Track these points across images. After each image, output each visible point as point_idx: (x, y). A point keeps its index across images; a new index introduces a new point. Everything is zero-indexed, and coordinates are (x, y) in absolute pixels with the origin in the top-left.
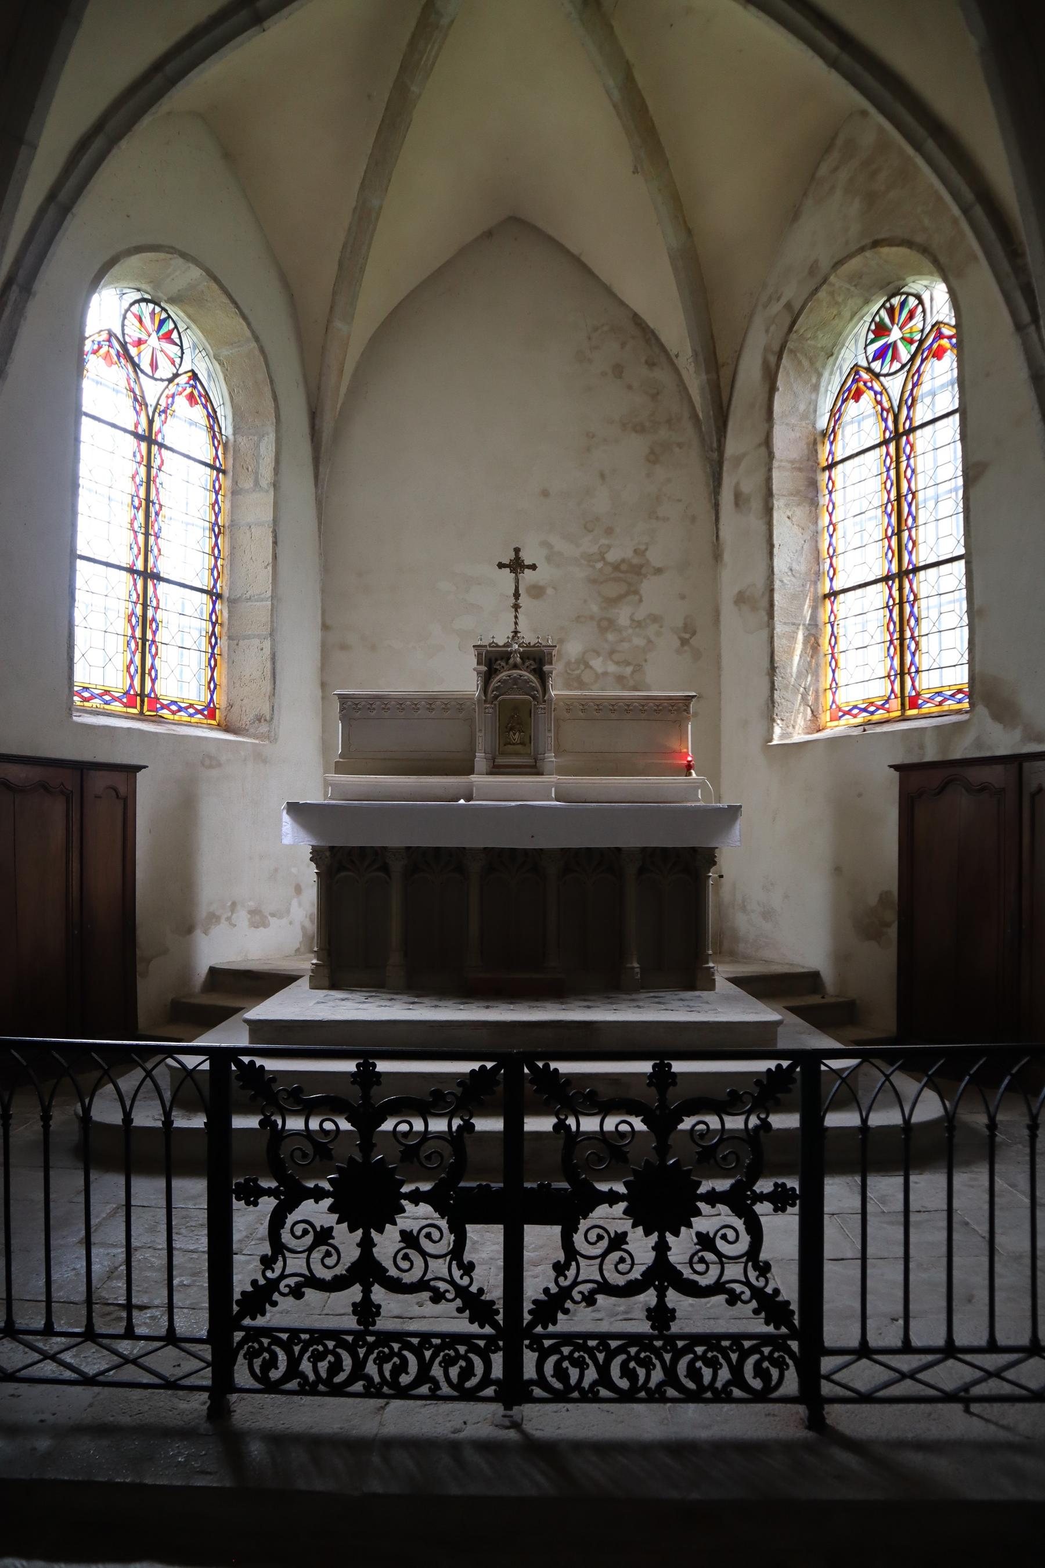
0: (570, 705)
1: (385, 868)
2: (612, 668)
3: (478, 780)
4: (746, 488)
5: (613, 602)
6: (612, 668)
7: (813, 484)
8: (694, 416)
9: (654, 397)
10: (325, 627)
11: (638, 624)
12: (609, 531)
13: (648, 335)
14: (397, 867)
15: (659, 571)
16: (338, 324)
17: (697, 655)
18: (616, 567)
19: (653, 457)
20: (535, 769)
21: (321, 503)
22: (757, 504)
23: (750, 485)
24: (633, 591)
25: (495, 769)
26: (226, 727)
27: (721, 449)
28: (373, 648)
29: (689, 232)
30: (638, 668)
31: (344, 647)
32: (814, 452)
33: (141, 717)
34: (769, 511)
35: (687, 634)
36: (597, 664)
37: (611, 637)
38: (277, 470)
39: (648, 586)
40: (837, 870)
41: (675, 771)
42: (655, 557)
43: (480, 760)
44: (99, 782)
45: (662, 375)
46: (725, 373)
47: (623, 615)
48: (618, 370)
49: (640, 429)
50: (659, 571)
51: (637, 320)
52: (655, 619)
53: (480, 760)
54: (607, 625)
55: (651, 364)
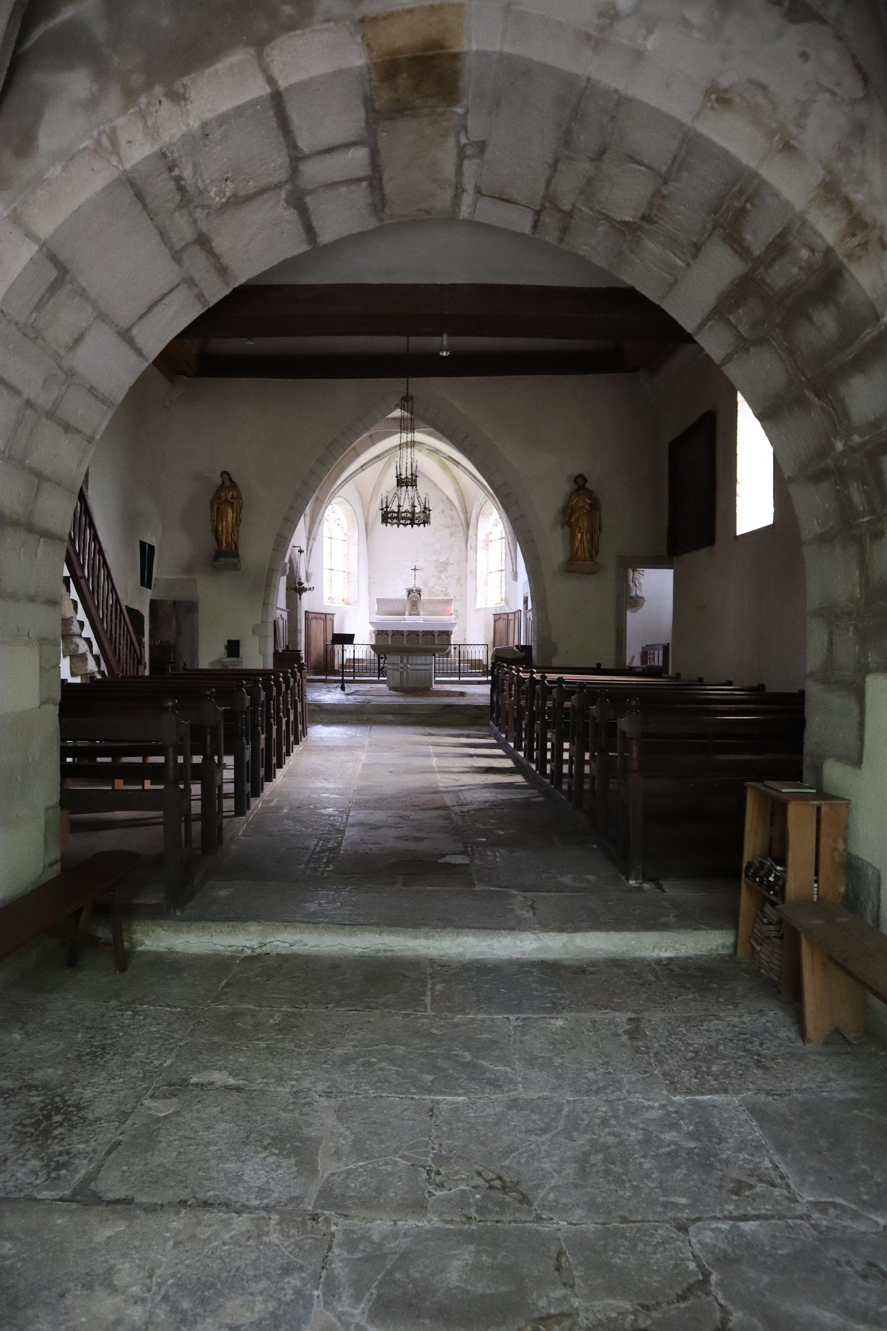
0: (427, 601)
1: (387, 635)
2: (440, 589)
3: (406, 617)
4: (473, 545)
5: (441, 572)
6: (440, 589)
7: (487, 545)
8: (462, 524)
9: (452, 519)
10: (369, 578)
11: (447, 578)
12: (440, 554)
13: (451, 502)
14: (390, 634)
15: (452, 564)
16: (373, 504)
17: (461, 585)
18: (442, 563)
19: (451, 535)
20: (418, 615)
21: (368, 546)
22: (474, 550)
23: (473, 545)
24: (445, 569)
25: (410, 615)
26: (347, 604)
27: (468, 534)
28: (837, 1031)
29: (458, 483)
30: (447, 589)
31: (374, 583)
32: (488, 537)
33: (331, 602)
34: (476, 552)
35: (459, 580)
36: (436, 588)
37: (440, 581)
38: (358, 541)
39: (450, 568)
40: (485, 637)
41: (449, 615)
42: (451, 561)
43: (407, 613)
44: (328, 617)
45: (454, 513)
46: (469, 515)
47: (443, 575)
48: (443, 511)
49: (448, 527)
50: (452, 564)
51: (448, 498)
52: (451, 576)
53: (407, 613)
54: (439, 578)
55: (451, 510)
